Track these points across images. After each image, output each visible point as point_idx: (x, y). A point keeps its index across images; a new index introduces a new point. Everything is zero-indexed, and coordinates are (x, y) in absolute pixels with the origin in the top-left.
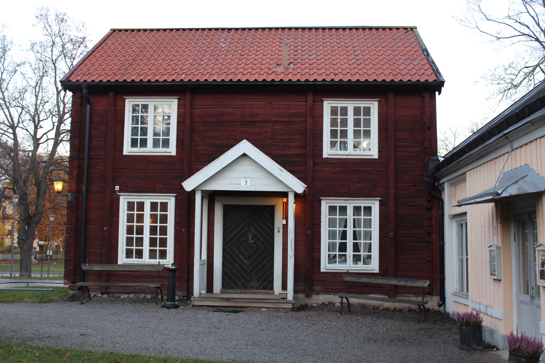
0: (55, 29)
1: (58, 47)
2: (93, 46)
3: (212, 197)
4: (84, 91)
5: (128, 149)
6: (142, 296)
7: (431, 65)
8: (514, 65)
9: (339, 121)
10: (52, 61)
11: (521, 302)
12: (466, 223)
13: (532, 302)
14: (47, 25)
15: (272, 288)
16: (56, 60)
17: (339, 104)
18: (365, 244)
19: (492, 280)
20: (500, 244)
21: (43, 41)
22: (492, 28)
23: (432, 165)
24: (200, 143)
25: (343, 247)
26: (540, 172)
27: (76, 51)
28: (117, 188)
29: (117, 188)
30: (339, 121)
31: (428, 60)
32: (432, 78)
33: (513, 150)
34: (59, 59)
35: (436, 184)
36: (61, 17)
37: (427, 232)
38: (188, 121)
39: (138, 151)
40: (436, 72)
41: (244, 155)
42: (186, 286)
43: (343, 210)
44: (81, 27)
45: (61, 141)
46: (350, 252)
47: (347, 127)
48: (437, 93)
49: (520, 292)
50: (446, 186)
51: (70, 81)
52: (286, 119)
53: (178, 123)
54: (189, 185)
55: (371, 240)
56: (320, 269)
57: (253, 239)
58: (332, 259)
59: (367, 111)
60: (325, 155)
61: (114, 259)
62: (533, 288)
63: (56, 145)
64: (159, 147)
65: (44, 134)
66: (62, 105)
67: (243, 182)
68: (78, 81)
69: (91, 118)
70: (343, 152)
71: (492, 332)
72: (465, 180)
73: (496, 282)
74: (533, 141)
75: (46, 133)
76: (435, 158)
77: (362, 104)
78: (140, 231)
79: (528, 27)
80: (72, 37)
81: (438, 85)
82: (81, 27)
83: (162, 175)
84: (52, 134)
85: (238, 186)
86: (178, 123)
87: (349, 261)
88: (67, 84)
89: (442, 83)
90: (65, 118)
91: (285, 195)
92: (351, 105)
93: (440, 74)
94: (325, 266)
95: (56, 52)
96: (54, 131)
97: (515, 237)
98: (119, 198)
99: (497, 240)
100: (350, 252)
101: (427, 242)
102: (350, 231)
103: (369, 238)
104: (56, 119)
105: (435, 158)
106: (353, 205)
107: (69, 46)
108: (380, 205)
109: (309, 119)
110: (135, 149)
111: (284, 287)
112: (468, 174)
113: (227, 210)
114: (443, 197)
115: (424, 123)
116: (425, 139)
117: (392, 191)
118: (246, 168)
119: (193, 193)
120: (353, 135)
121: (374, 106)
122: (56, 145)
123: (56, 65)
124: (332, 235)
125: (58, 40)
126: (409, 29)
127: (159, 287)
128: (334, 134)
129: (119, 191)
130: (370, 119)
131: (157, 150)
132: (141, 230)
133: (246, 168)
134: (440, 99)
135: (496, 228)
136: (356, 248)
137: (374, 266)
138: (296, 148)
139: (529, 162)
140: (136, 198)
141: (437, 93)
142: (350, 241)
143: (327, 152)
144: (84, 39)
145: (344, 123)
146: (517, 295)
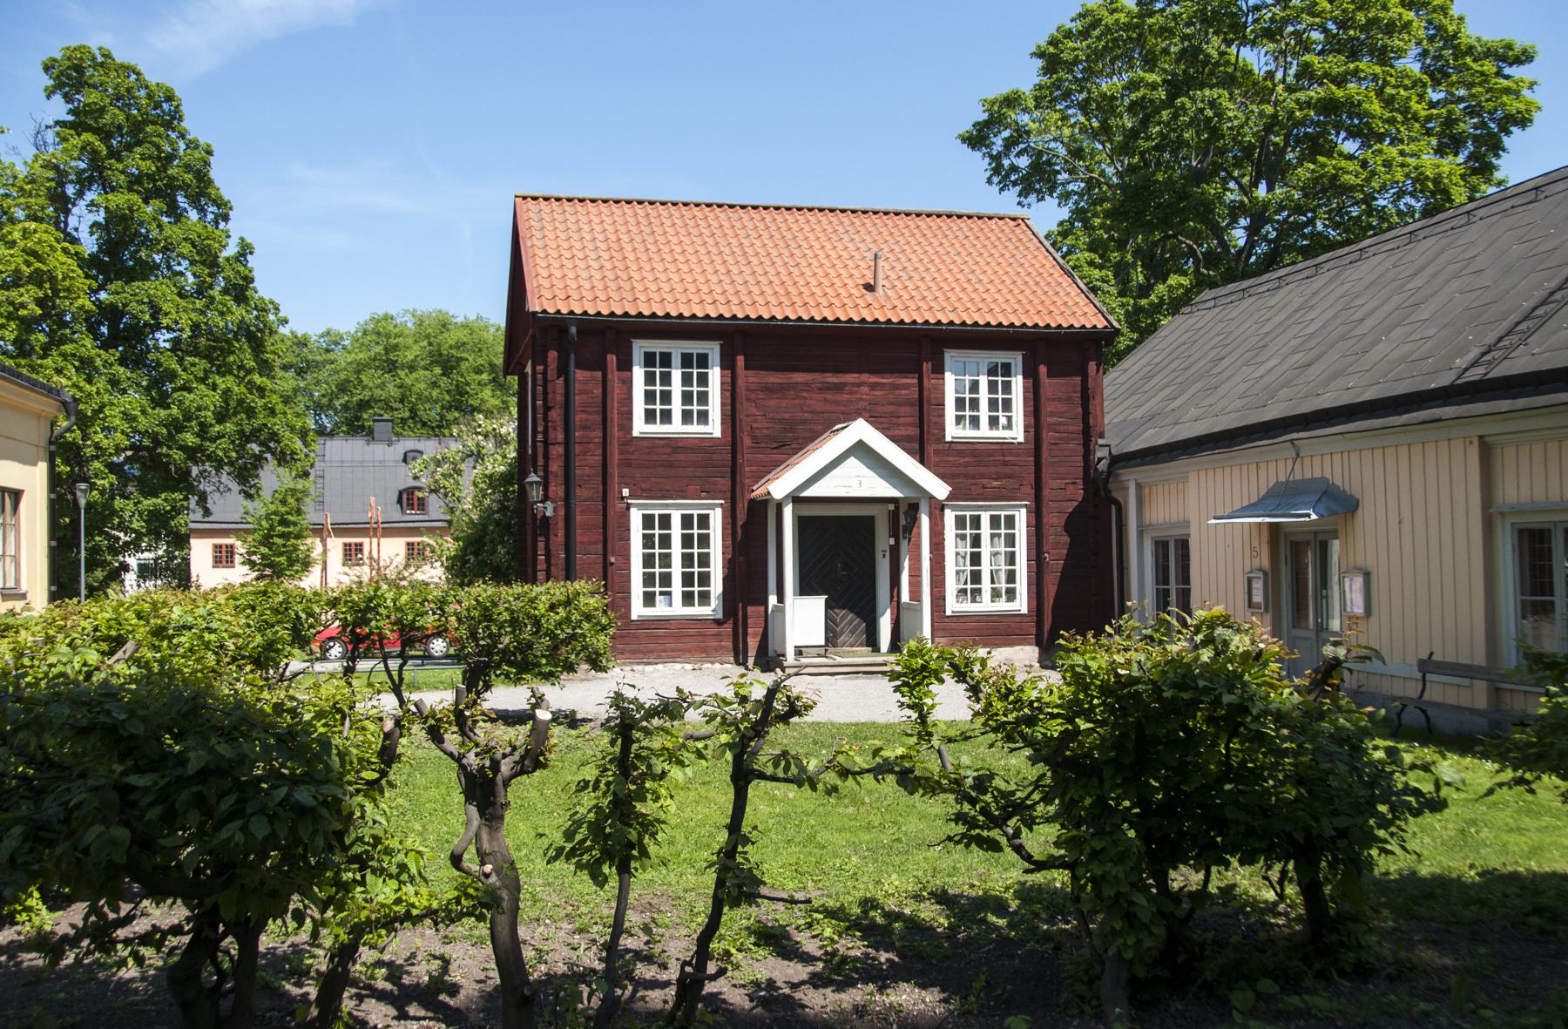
5: (640, 427)
29: (626, 492)
60: (636, 433)
67: (855, 483)
70: (665, 428)
112: (1193, 477)
118: (844, 464)
133: (844, 464)
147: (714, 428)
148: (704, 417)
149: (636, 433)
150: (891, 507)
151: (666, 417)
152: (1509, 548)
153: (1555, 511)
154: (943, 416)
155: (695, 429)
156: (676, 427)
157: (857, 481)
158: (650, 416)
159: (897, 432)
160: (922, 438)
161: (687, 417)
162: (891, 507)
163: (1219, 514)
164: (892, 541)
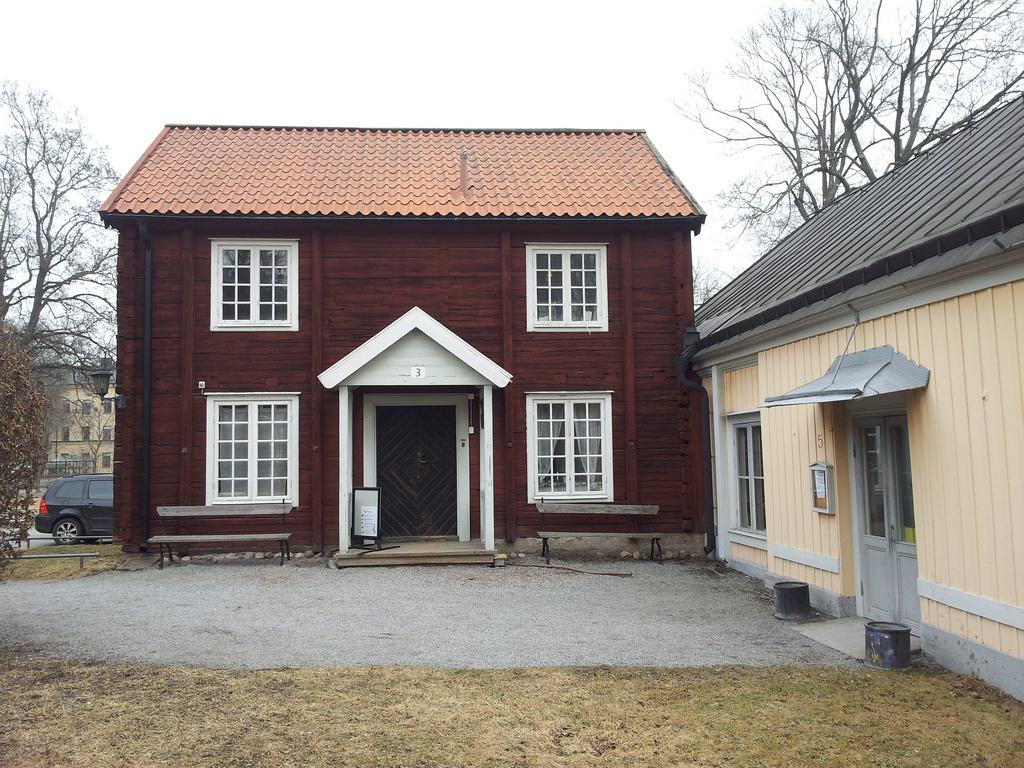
0: (30, 117)
1: (35, 147)
2: (138, 158)
3: (359, 394)
4: (142, 228)
5: (217, 322)
6: (249, 555)
7: (680, 190)
8: (752, 181)
9: (550, 275)
10: (27, 168)
11: (866, 549)
12: (757, 430)
13: (891, 547)
14: (15, 112)
15: (455, 532)
16: (33, 168)
17: (550, 250)
18: (592, 459)
19: (816, 515)
20: (832, 461)
21: (8, 134)
22: (723, 124)
23: (688, 341)
24: (344, 309)
25: (559, 465)
26: (915, 359)
27: (65, 154)
28: (202, 384)
29: (202, 384)
30: (550, 275)
31: (674, 183)
32: (686, 211)
33: (859, 324)
34: (39, 167)
35: (694, 369)
36: (39, 98)
37: (683, 440)
38: (317, 278)
39: (236, 324)
40: (691, 202)
41: (416, 332)
42: (320, 536)
43: (559, 410)
44: (72, 115)
45: (48, 300)
46: (570, 472)
47: (561, 285)
48: (692, 233)
49: (866, 533)
50: (714, 372)
51: (116, 211)
52: (471, 274)
53: (300, 279)
54: (329, 378)
55: (600, 453)
56: (527, 500)
57: (423, 458)
58: (544, 484)
59: (591, 261)
60: (530, 328)
61: (200, 499)
62: (892, 528)
63: (38, 307)
64: (270, 318)
65: (15, 290)
66: (44, 240)
67: (414, 371)
68: (130, 211)
69: (152, 272)
70: (244, 322)
71: (821, 595)
72: (755, 363)
73: (825, 521)
74: (891, 315)
75: (18, 288)
76: (690, 330)
77: (583, 250)
78: (242, 450)
79: (766, 126)
80: (59, 131)
81: (696, 221)
82: (72, 115)
83: (283, 364)
84: (30, 289)
85: (405, 378)
86: (299, 279)
87: (571, 486)
88: (110, 218)
89: (702, 218)
90: (53, 262)
91: (476, 391)
92: (566, 252)
93: (696, 203)
94: (534, 494)
95: (33, 157)
96: (34, 283)
97: (855, 451)
98: (205, 401)
99: (826, 455)
100: (570, 472)
101: (683, 455)
102: (569, 441)
103: (597, 450)
104: (35, 263)
105: (690, 330)
106: (573, 402)
107: (53, 145)
108: (613, 401)
109: (505, 274)
110: (229, 323)
111: (475, 530)
112: (761, 356)
113: (384, 416)
114: (705, 385)
115: (675, 278)
116: (676, 302)
117: (630, 380)
118: (416, 351)
119: (334, 393)
120: (569, 300)
121: (601, 254)
122: (38, 307)
123: (35, 178)
124: (543, 447)
125: (35, 134)
126: (635, 134)
127: (286, 541)
128: (542, 296)
129: (205, 390)
130: (595, 273)
131: (267, 323)
132: (248, 450)
133: (416, 351)
134: (697, 242)
135: (822, 437)
136: (579, 465)
137: (607, 492)
138: (490, 321)
139: (892, 343)
140: (233, 400)
141: (692, 233)
142: (570, 456)
143: (533, 323)
144: (79, 134)
145: (557, 279)
146: (860, 537)
147: (292, 323)
148: (282, 313)
149: (530, 328)
150: (471, 397)
151: (245, 312)
152: (859, 566)
153: (471, 564)
154: (524, 307)
155: (273, 324)
156: (254, 322)
157: (417, 370)
158: (228, 313)
159: (460, 325)
160: (495, 331)
161: (265, 313)
162: (471, 397)
163: (772, 395)
164: (472, 430)
